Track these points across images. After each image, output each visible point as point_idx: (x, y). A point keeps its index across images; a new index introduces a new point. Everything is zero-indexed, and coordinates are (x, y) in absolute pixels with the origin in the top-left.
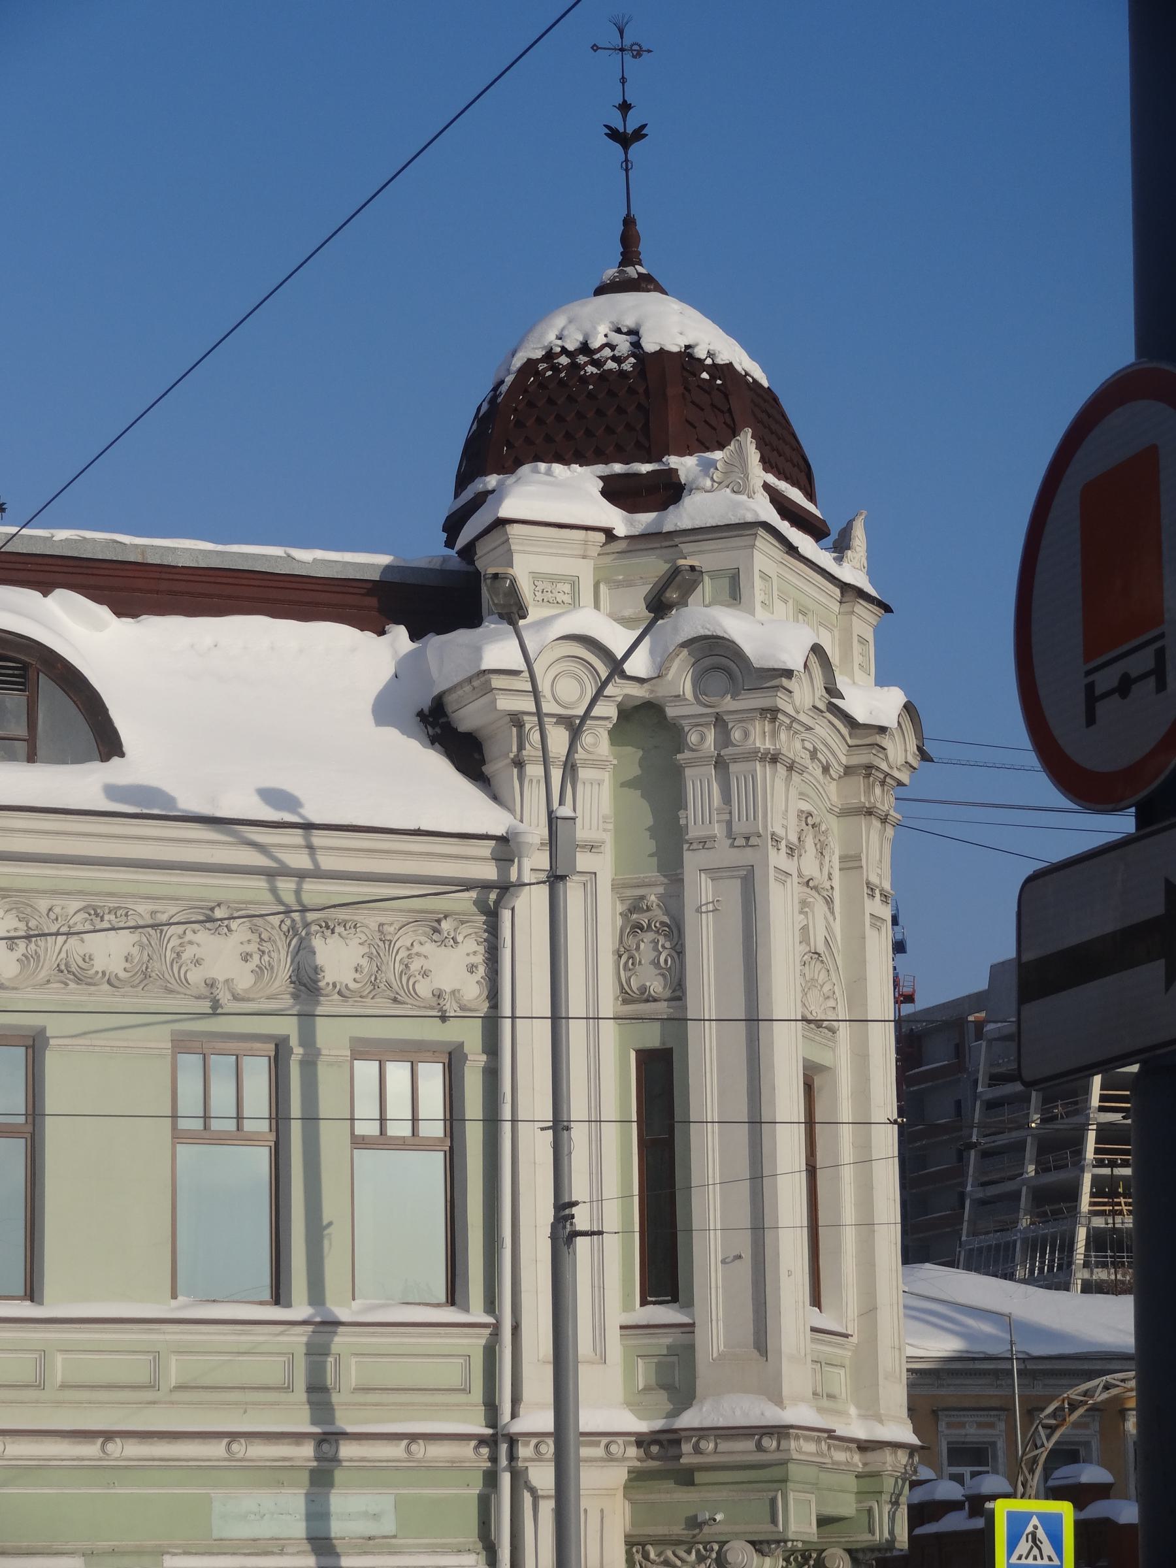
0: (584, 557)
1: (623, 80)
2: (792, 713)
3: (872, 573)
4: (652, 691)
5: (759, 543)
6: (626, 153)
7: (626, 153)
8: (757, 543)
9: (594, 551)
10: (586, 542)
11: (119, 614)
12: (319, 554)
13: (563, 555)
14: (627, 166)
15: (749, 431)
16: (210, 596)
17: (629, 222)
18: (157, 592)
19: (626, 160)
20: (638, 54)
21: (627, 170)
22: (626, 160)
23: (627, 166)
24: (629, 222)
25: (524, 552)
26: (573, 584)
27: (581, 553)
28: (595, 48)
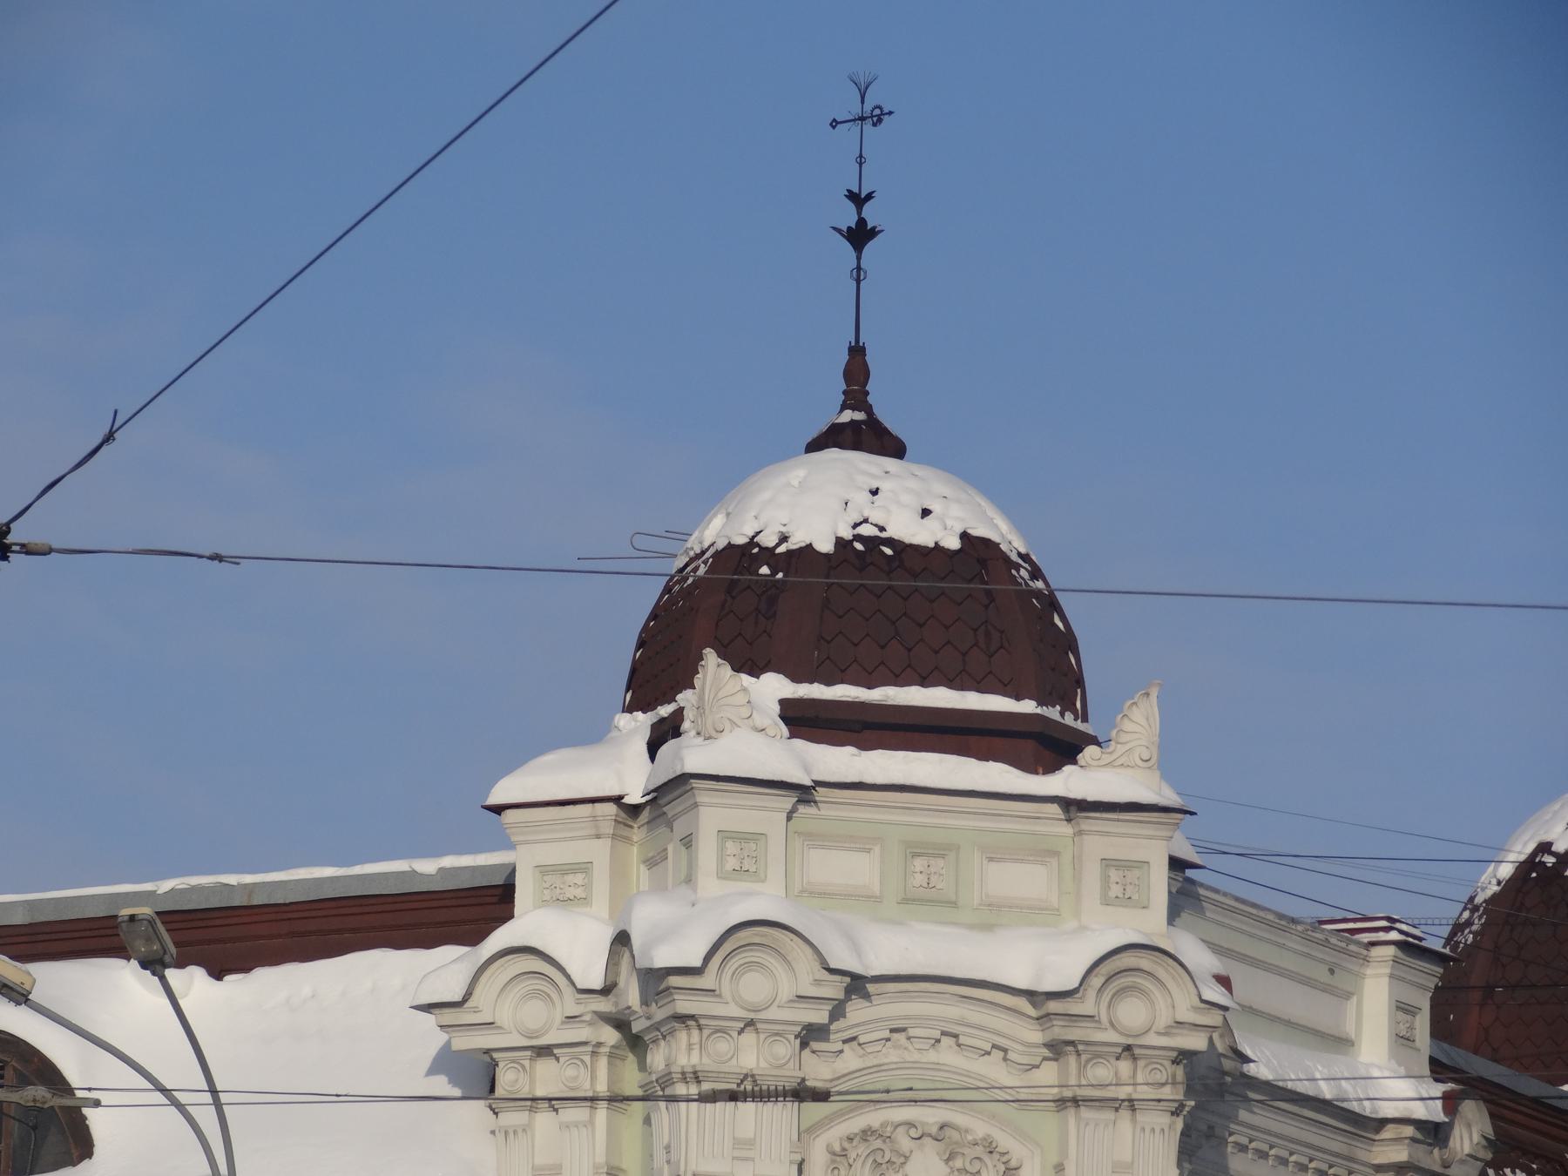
0: (598, 837)
1: (861, 160)
2: (648, 1023)
3: (1167, 762)
4: (616, 1004)
5: (702, 798)
6: (859, 258)
7: (859, 258)
8: (699, 799)
9: (608, 828)
10: (594, 818)
11: (218, 974)
12: (449, 861)
13: (572, 839)
14: (858, 274)
15: (710, 657)
16: (339, 931)
17: (857, 352)
18: (280, 936)
19: (859, 268)
20: (879, 121)
21: (858, 281)
22: (859, 268)
23: (858, 274)
24: (857, 352)
25: (527, 842)
26: (915, 855)
27: (593, 832)
28: (834, 124)
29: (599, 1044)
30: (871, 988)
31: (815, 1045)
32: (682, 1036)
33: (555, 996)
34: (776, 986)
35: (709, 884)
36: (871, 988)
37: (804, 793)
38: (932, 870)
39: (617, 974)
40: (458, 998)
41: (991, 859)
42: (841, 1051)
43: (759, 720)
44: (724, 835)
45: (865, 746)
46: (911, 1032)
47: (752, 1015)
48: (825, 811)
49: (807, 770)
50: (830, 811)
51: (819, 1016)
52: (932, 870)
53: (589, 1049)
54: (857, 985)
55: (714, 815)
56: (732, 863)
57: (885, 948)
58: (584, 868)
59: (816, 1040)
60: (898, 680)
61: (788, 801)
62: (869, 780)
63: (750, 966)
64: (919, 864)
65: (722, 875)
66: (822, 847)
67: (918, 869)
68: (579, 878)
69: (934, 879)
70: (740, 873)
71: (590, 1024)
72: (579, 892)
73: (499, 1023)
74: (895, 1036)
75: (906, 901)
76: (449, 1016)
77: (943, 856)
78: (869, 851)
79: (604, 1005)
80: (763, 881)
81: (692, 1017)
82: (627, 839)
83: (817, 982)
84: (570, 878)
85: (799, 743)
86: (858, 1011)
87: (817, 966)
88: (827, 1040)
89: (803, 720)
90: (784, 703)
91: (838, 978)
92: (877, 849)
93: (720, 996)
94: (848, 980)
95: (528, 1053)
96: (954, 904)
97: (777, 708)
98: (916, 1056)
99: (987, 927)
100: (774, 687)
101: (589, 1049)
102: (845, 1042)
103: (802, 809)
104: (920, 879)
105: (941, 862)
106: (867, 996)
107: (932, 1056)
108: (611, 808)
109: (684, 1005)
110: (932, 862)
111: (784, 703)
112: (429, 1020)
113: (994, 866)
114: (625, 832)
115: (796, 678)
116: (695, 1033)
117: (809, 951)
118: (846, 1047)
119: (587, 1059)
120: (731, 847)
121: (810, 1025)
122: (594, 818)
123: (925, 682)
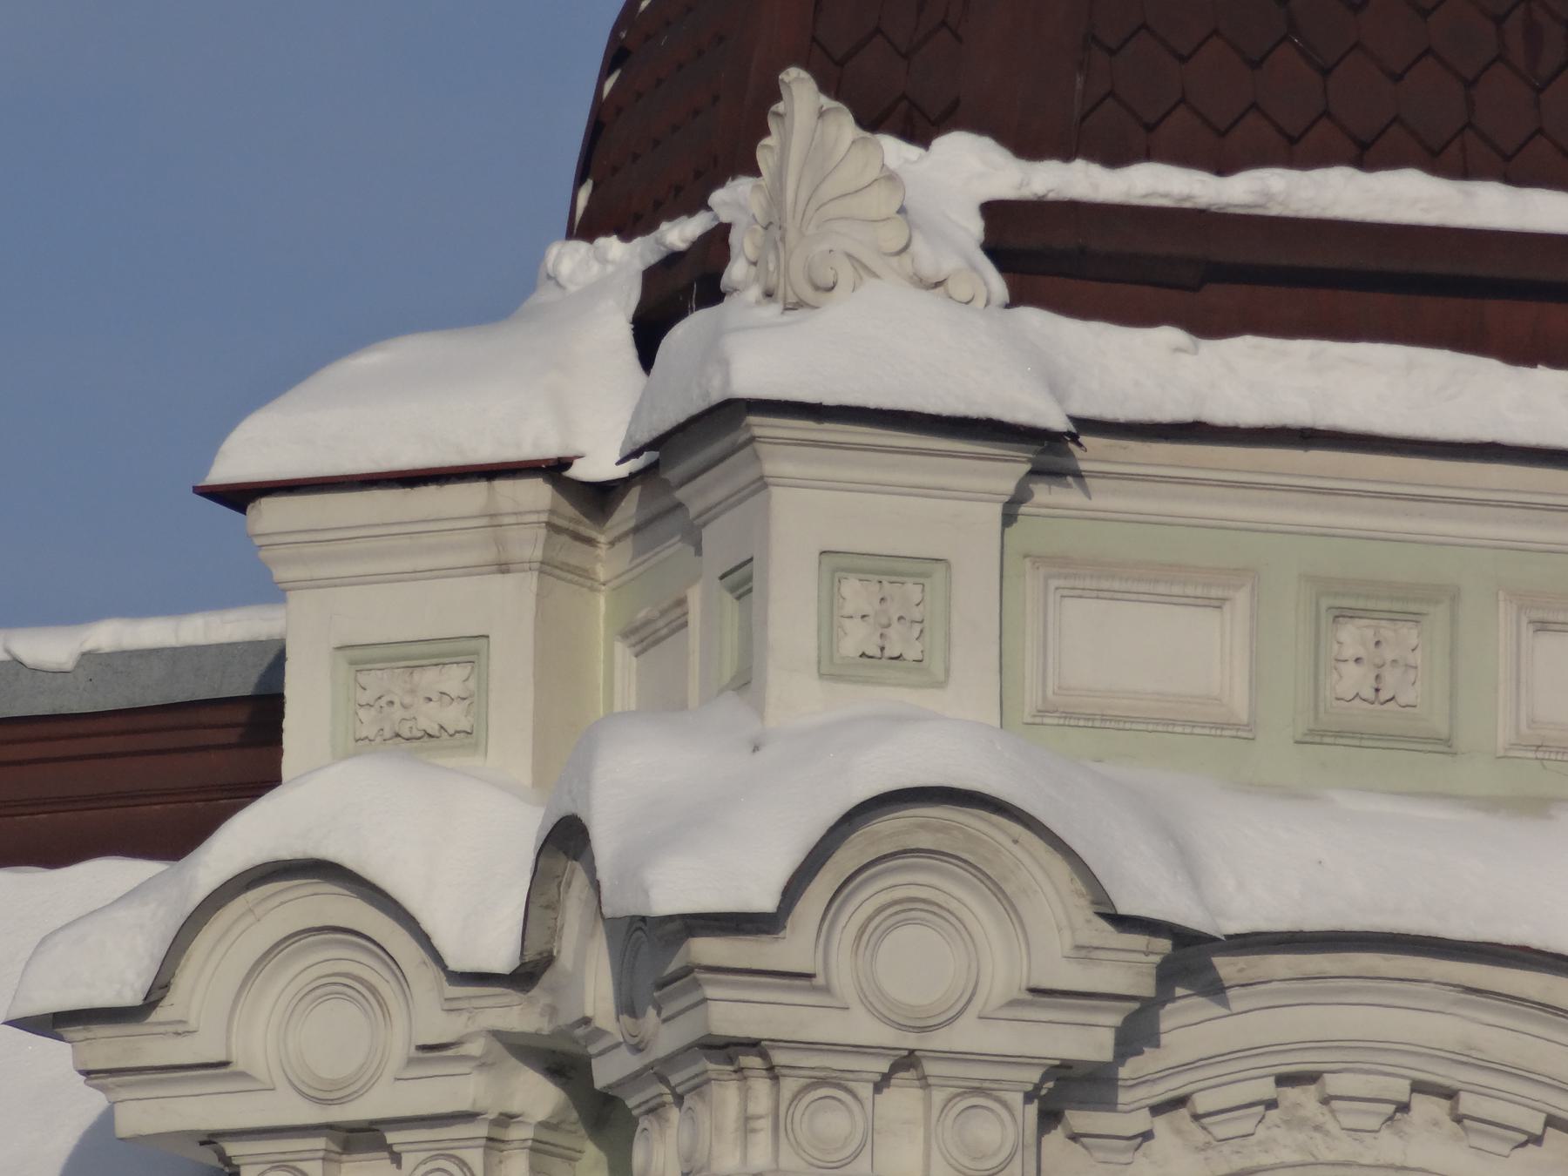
0: (503, 568)
9: (529, 545)
10: (493, 519)
26: (1342, 615)
29: (506, 1119)
30: (1227, 967)
31: (1078, 1119)
32: (727, 1095)
33: (388, 989)
34: (974, 963)
35: (796, 695)
36: (1227, 967)
37: (1048, 451)
38: (1388, 654)
39: (555, 932)
40: (132, 996)
41: (1542, 626)
42: (1147, 1136)
43: (928, 259)
44: (837, 564)
45: (1207, 326)
46: (1334, 1084)
47: (911, 1041)
48: (1106, 499)
49: (1055, 388)
50: (1117, 498)
51: (1090, 1042)
52: (1388, 654)
53: (480, 1130)
54: (1192, 958)
55: (810, 506)
56: (856, 638)
57: (1263, 864)
58: (466, 651)
59: (1084, 1104)
60: (1298, 152)
61: (1004, 471)
62: (1219, 414)
63: (906, 909)
64: (1352, 637)
65: (832, 670)
66: (1099, 594)
67: (1349, 652)
68: (453, 679)
69: (1391, 678)
70: (880, 662)
71: (483, 1064)
72: (454, 717)
73: (240, 1065)
74: (1291, 1094)
75: (1315, 736)
76: (108, 1046)
77: (1415, 618)
78: (1218, 604)
79: (519, 1015)
80: (941, 685)
81: (753, 1045)
82: (584, 575)
83: (1084, 953)
84: (429, 679)
85: (1033, 318)
86: (1189, 1029)
87: (1082, 911)
88: (1110, 1105)
89: (1038, 256)
90: (993, 211)
91: (1138, 940)
92: (1242, 598)
93: (826, 990)
94: (1164, 945)
95: (320, 1143)
96: (1445, 745)
97: (975, 227)
98: (1345, 1148)
99: (1535, 806)
100: (968, 171)
101: (480, 1130)
102: (1156, 1110)
103: (1045, 494)
104: (1354, 679)
105: (1410, 634)
106: (1215, 989)
107: (1388, 1147)
108: (537, 493)
109: (733, 1013)
110: (1387, 631)
111: (993, 211)
112: (56, 1055)
113: (1547, 641)
114: (575, 554)
115: (1027, 146)
116: (761, 1087)
117: (1060, 867)
118: (1161, 1124)
119: (475, 1157)
120: (856, 595)
121: (1066, 1065)
122: (493, 519)
123: (1368, 154)
